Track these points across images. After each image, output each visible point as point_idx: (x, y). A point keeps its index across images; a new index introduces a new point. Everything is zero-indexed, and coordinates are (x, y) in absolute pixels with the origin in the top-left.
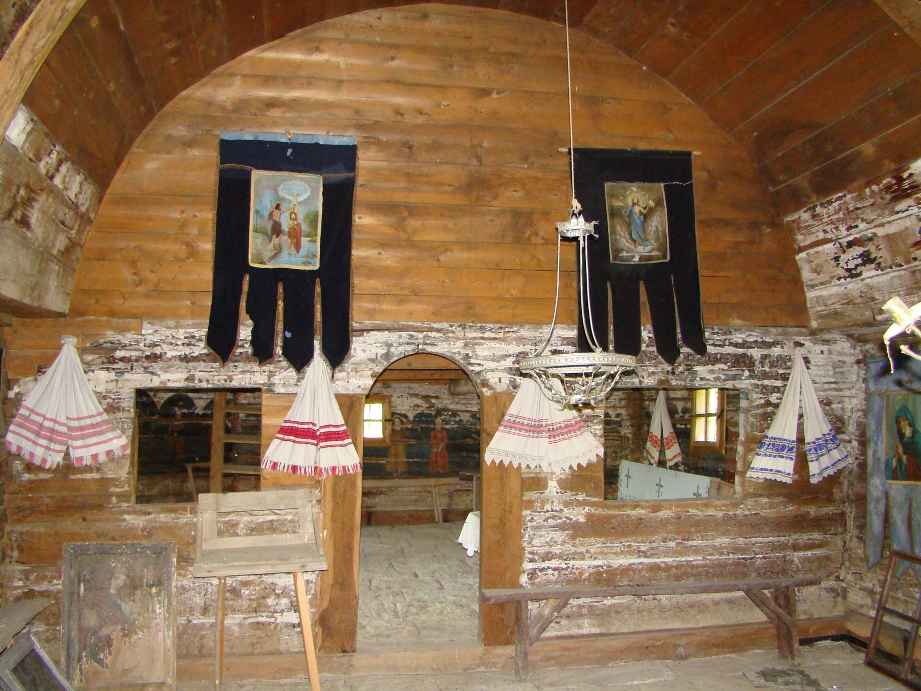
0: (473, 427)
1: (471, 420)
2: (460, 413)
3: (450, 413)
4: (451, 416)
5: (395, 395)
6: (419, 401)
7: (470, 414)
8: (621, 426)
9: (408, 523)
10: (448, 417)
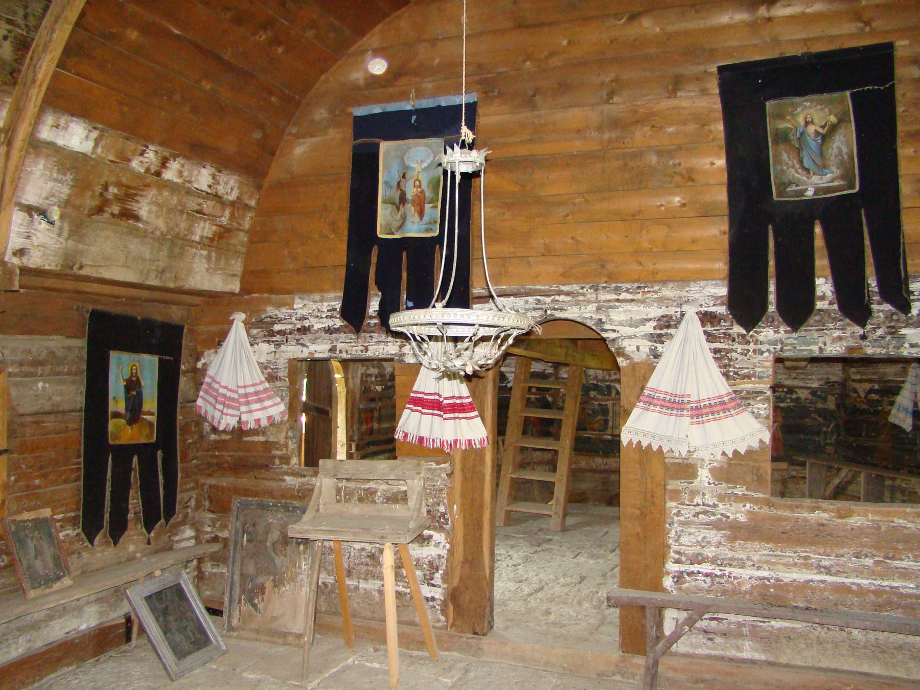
1: (810, 397)
3: (785, 390)
4: (786, 393)
7: (809, 391)
10: (783, 394)
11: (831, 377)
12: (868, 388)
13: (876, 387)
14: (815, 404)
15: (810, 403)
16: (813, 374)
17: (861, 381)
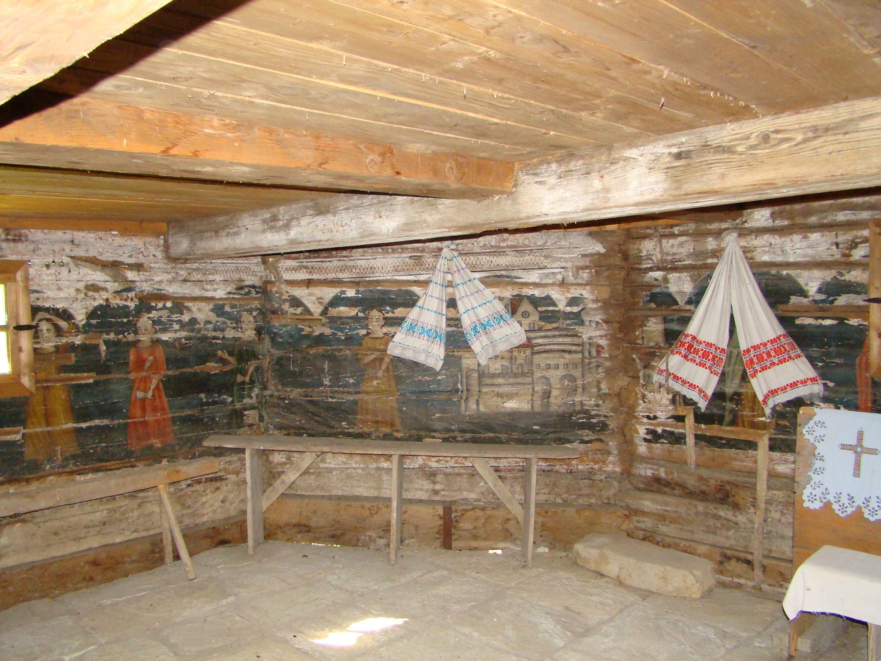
0: (219, 334)
1: (213, 317)
2: (190, 304)
3: (169, 304)
4: (171, 311)
5: (36, 260)
6: (98, 276)
7: (211, 306)
8: (582, 323)
9: (90, 580)
10: (165, 313)
11: (244, 276)
12: (332, 295)
13: (351, 293)
14: (223, 330)
15: (215, 330)
16: (216, 271)
17: (309, 283)
